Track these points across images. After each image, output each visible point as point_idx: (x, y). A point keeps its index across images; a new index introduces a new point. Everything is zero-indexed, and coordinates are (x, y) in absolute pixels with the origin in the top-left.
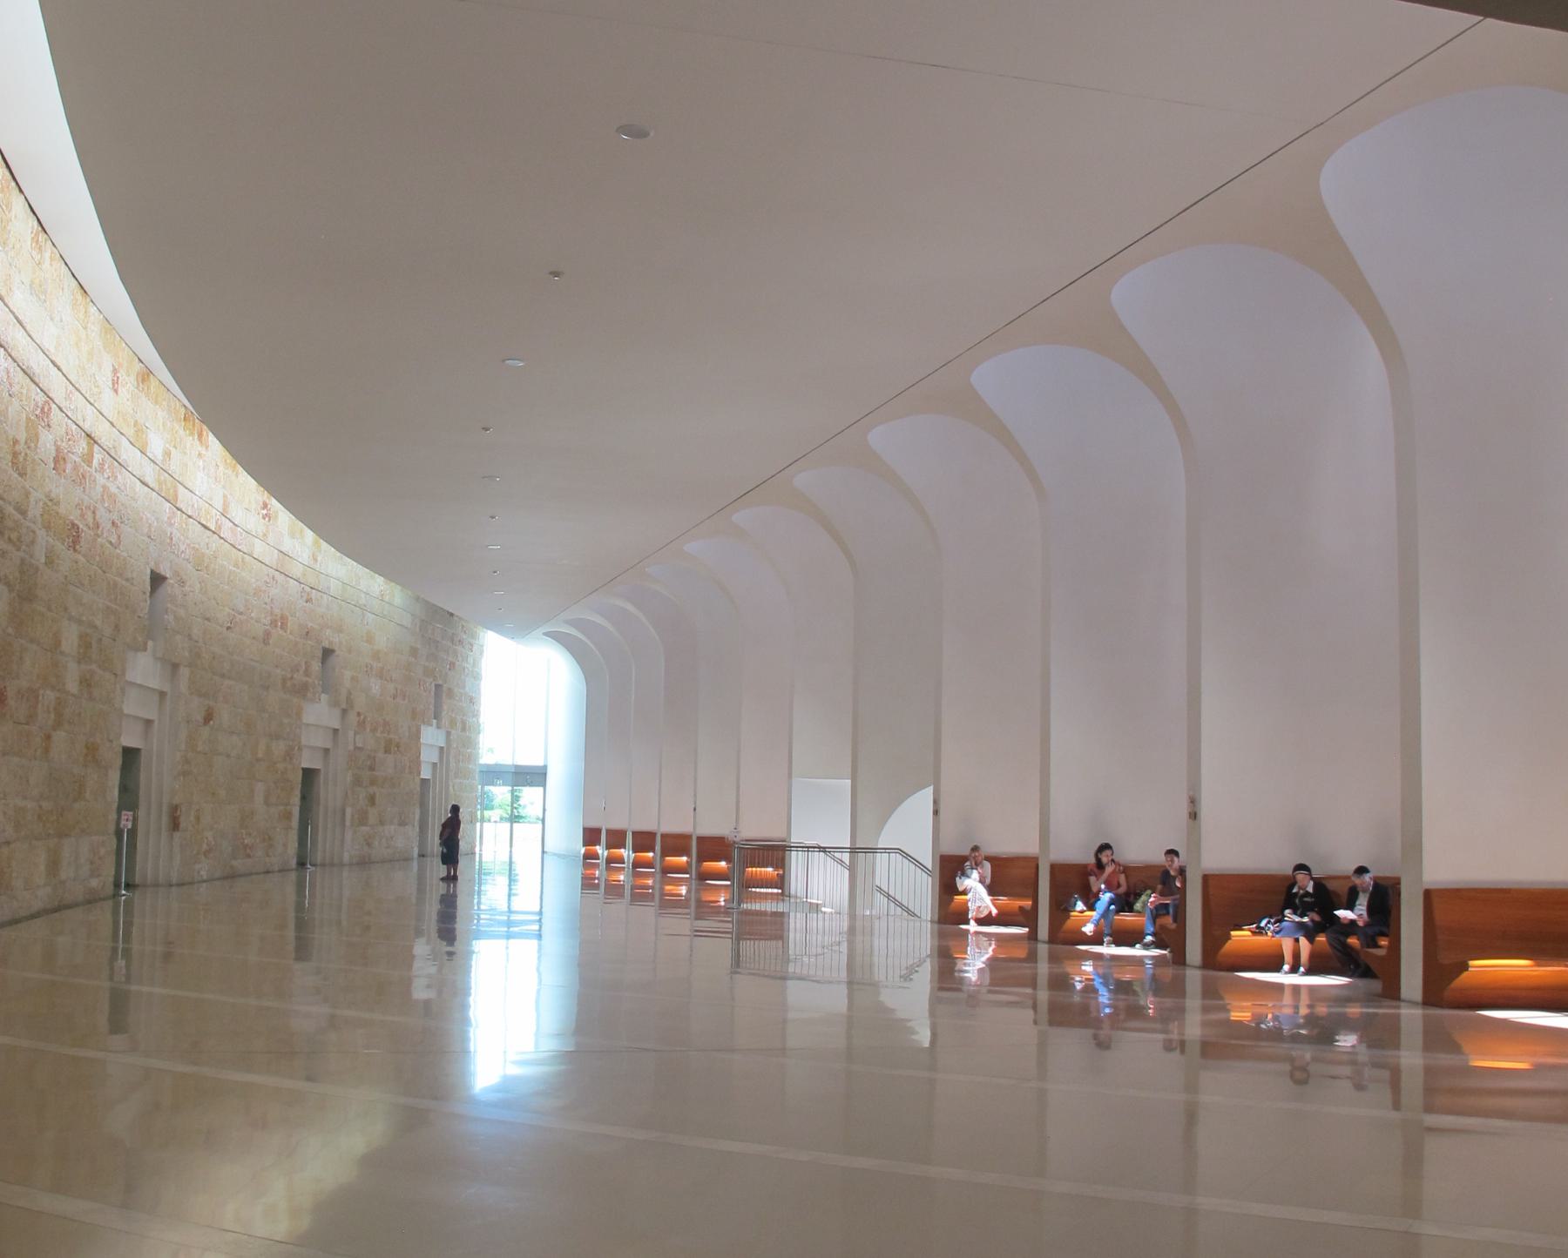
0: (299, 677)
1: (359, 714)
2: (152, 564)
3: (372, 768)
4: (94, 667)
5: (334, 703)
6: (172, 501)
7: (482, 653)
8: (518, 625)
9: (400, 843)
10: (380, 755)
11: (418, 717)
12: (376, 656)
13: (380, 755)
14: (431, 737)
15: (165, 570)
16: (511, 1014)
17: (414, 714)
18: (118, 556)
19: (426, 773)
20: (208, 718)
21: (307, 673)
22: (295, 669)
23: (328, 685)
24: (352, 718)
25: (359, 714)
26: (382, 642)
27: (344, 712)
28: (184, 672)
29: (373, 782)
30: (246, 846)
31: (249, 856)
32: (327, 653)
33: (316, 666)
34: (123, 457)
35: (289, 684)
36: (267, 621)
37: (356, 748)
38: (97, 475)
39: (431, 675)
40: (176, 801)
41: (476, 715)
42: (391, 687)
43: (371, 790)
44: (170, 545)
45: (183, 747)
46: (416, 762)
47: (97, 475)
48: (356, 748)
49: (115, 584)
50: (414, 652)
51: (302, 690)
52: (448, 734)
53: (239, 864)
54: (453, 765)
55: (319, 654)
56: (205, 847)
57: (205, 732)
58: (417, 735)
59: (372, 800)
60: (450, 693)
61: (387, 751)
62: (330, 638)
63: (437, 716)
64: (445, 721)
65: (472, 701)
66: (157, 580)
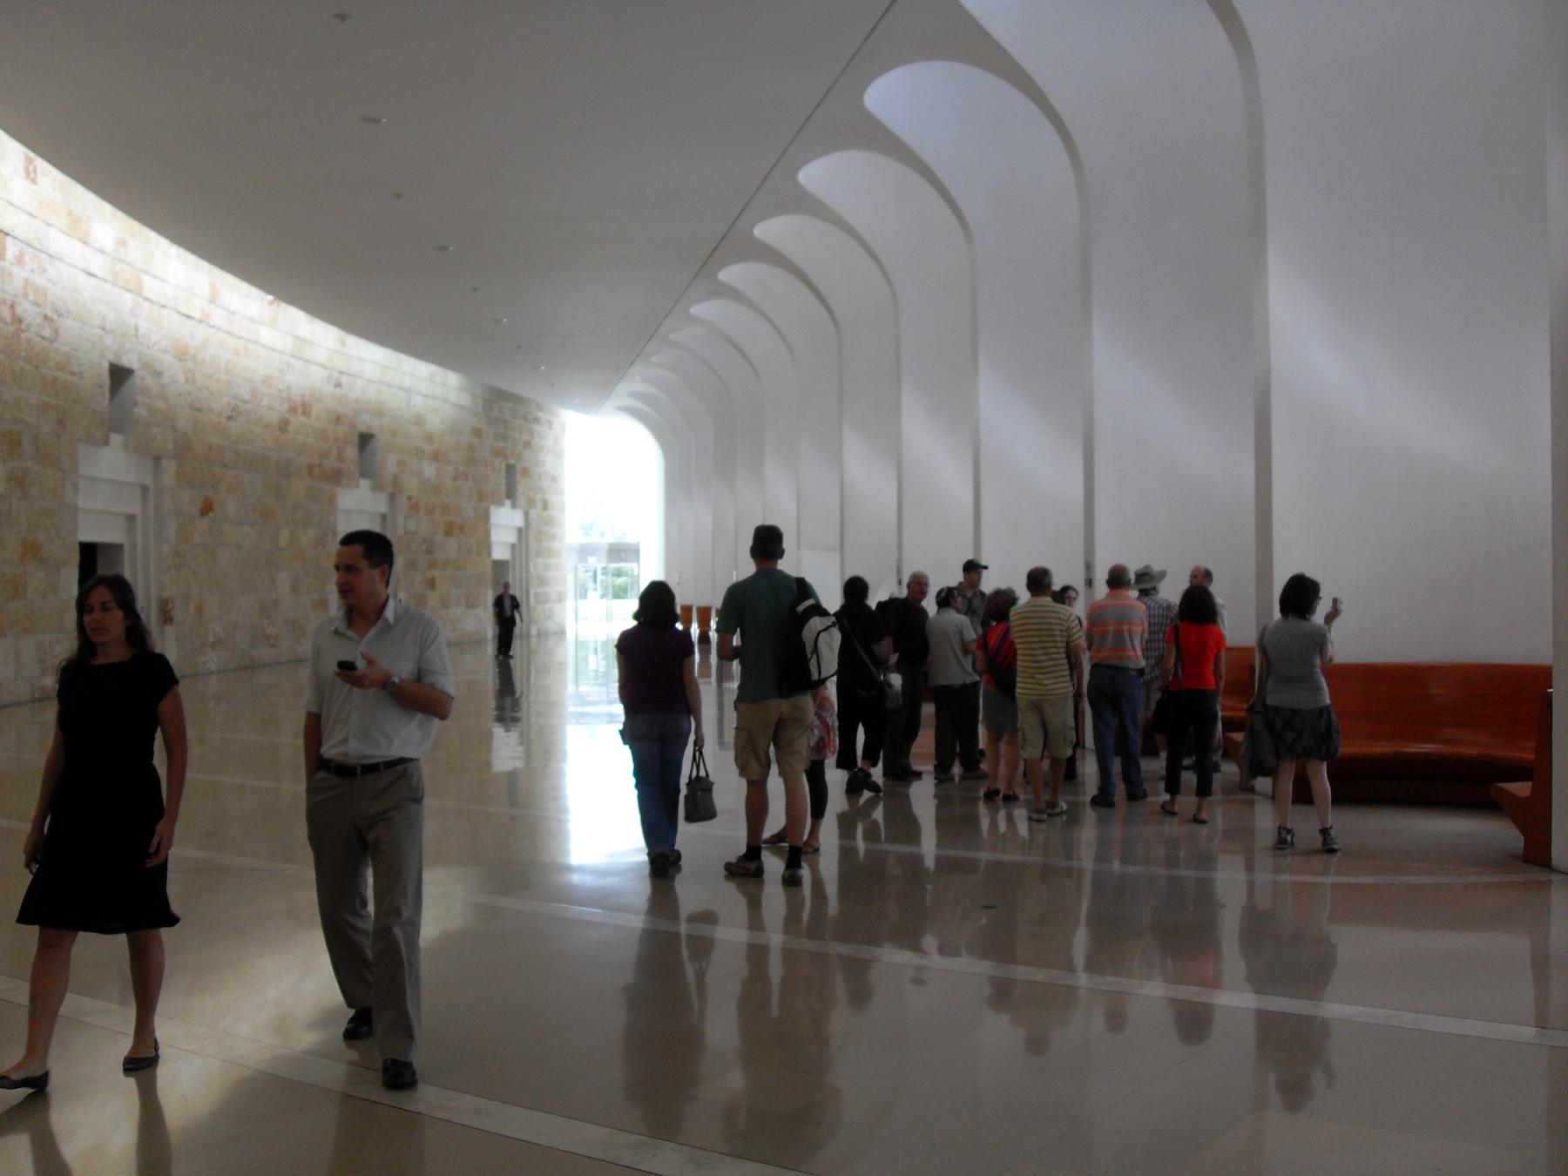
0: (331, 463)
1: (409, 498)
2: (111, 357)
3: (430, 552)
4: (29, 463)
5: (377, 488)
6: (137, 291)
7: (563, 429)
8: (869, 608)
9: (469, 625)
10: (440, 538)
11: (485, 500)
12: (429, 438)
13: (440, 538)
14: (504, 523)
15: (129, 361)
16: (775, 1011)
17: (481, 496)
18: (57, 351)
19: (500, 553)
20: (207, 508)
21: (340, 458)
22: (325, 454)
23: (367, 470)
24: (402, 501)
25: (409, 498)
26: (435, 423)
27: (392, 497)
28: (170, 467)
29: (432, 565)
30: (268, 637)
31: (273, 646)
32: (365, 440)
33: (351, 452)
34: (53, 248)
35: (317, 471)
36: (285, 406)
37: (407, 532)
38: (16, 270)
39: (497, 453)
40: (167, 594)
41: (560, 493)
42: (450, 469)
43: (429, 574)
44: (136, 336)
45: (172, 539)
46: (486, 545)
47: (16, 270)
48: (407, 532)
49: (55, 381)
50: (477, 432)
51: (336, 477)
52: (526, 514)
53: (263, 653)
54: (533, 544)
55: (356, 439)
56: (211, 639)
57: (203, 525)
58: (486, 517)
59: (431, 584)
60: (526, 473)
61: (448, 533)
62: (366, 423)
63: (511, 495)
64: (521, 500)
65: (554, 479)
66: (119, 375)
